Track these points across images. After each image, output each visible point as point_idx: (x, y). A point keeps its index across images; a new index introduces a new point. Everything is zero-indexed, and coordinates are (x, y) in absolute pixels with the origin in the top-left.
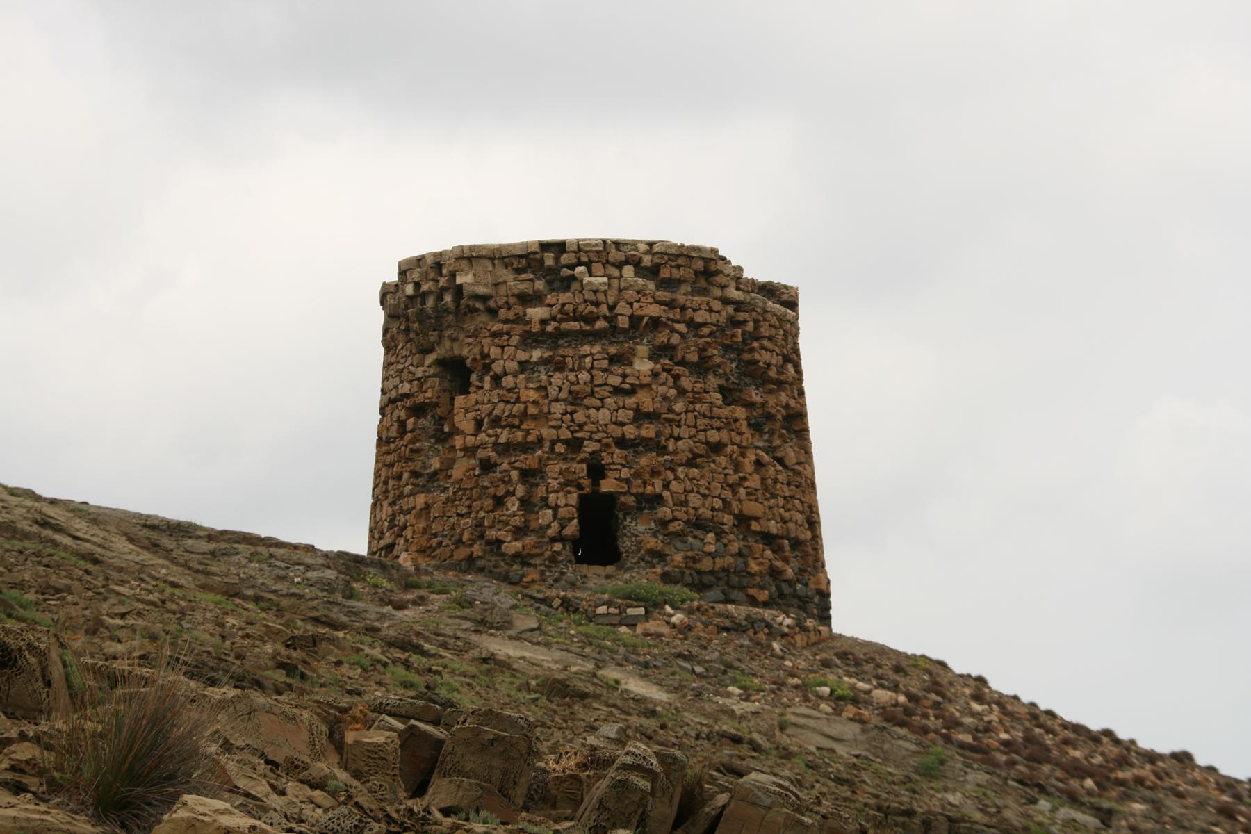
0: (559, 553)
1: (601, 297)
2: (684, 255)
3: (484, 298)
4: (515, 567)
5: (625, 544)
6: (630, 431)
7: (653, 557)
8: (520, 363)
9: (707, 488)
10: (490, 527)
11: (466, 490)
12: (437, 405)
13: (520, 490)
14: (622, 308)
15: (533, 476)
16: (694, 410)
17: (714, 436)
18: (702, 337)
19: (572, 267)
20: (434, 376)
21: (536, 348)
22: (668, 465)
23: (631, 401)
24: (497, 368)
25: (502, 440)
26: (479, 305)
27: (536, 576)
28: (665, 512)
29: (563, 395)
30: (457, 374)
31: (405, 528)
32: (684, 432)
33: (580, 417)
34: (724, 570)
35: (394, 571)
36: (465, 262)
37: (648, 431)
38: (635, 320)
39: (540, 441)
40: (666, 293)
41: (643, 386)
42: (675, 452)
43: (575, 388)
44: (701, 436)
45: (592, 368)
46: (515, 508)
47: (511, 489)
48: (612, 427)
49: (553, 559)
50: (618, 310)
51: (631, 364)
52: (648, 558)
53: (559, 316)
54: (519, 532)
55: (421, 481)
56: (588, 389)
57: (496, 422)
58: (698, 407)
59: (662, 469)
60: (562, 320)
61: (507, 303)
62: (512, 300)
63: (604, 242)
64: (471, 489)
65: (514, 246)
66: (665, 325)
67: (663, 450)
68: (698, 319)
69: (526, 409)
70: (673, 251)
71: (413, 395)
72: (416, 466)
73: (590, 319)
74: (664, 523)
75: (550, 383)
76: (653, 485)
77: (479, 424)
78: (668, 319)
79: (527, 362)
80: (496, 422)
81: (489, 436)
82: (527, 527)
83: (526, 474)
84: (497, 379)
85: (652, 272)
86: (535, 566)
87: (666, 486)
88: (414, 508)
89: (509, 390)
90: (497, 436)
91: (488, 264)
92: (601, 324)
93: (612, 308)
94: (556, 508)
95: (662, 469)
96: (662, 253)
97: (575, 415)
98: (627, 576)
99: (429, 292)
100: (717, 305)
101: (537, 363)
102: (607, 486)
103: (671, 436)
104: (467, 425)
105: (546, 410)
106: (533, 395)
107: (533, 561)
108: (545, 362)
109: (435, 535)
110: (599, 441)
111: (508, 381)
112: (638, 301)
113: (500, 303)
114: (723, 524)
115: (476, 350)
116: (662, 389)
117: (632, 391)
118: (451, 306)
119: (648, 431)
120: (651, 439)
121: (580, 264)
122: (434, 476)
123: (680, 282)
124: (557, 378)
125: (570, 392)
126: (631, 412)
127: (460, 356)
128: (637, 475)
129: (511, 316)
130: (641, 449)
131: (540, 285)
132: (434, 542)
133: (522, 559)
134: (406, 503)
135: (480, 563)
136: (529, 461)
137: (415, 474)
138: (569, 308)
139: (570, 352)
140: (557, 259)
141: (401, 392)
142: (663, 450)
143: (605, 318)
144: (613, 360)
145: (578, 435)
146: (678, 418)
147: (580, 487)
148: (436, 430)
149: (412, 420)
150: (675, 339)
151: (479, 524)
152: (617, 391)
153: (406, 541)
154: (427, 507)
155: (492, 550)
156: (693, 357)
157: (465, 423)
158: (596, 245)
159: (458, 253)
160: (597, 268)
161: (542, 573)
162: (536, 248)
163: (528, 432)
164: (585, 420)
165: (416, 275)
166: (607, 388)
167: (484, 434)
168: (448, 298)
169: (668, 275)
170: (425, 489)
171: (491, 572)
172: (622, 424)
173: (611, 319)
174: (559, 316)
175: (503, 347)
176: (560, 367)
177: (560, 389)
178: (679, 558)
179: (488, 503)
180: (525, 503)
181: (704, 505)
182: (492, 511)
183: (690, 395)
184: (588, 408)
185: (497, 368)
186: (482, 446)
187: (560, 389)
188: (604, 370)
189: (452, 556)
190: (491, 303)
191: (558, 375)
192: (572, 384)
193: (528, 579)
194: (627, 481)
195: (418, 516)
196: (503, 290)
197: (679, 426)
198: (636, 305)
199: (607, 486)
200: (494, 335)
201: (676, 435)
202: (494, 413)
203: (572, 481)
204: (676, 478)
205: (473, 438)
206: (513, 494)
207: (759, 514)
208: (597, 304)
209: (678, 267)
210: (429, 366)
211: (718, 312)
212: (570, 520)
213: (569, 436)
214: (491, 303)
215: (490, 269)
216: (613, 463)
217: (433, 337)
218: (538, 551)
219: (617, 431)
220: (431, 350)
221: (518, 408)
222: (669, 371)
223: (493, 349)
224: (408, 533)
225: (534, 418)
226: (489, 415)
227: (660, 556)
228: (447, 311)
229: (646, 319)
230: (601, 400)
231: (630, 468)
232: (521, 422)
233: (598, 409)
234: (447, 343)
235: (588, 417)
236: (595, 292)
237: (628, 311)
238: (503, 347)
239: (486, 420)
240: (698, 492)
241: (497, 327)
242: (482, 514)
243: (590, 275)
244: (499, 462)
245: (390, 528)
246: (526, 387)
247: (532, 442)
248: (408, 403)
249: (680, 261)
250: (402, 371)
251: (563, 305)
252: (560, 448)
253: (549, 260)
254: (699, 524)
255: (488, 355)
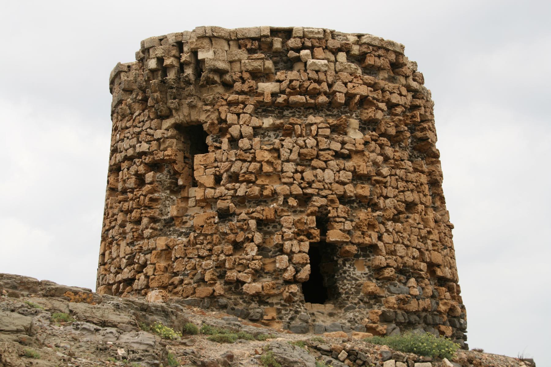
0: (294, 294)
1: (322, 76)
2: (383, 47)
3: (221, 72)
4: (253, 305)
5: (345, 286)
6: (350, 190)
7: (370, 299)
8: (254, 128)
9: (409, 240)
10: (231, 269)
11: (206, 235)
12: (174, 162)
13: (258, 237)
14: (338, 86)
15: (266, 225)
16: (396, 175)
17: (410, 197)
18: (396, 115)
19: (298, 50)
20: (172, 137)
21: (267, 117)
22: (381, 219)
23: (349, 164)
24: (234, 131)
25: (241, 192)
26: (217, 78)
27: (274, 314)
28: (380, 260)
29: (294, 156)
30: (194, 138)
31: (145, 265)
32: (390, 192)
33: (309, 175)
34: (425, 310)
35: (174, 318)
36: (206, 42)
37: (365, 190)
38: (349, 97)
39: (275, 193)
40: (371, 77)
41: (357, 152)
42: (384, 209)
43: (302, 151)
44: (401, 196)
45: (317, 135)
46: (254, 253)
47: (250, 236)
48: (335, 186)
49: (289, 300)
50: (336, 87)
51: (346, 134)
52: (366, 299)
53: (288, 90)
54: (257, 274)
55: (158, 226)
56: (315, 153)
57: (234, 178)
58: (398, 172)
59: (377, 223)
60: (290, 94)
61: (241, 78)
62: (246, 75)
63: (325, 31)
64: (212, 235)
65: (249, 30)
66: (374, 104)
67: (375, 207)
68: (394, 101)
69: (262, 166)
70: (376, 43)
71: (151, 153)
72: (155, 213)
73: (315, 94)
74: (379, 270)
75: (282, 146)
76: (370, 236)
77: (218, 179)
78: (374, 98)
79: (260, 127)
80: (234, 178)
81: (228, 189)
82: (263, 269)
83: (260, 223)
84: (234, 142)
85: (360, 59)
86: (272, 305)
87: (380, 238)
88: (155, 249)
89: (246, 151)
90: (236, 191)
91: (225, 44)
92: (322, 99)
93: (330, 86)
94: (291, 254)
95: (377, 223)
96: (369, 44)
97: (304, 174)
98: (350, 315)
99: (172, 66)
100: (404, 91)
101: (267, 130)
102: (334, 235)
103: (381, 195)
104: (207, 179)
105: (279, 169)
106: (267, 156)
107: (270, 301)
108: (275, 128)
109: (176, 274)
110: (325, 197)
111: (244, 143)
112: (351, 82)
113: (235, 77)
114: (421, 270)
115: (214, 116)
116: (373, 156)
117: (347, 157)
118: (192, 78)
119: (365, 190)
120: (366, 197)
121: (304, 47)
122: (170, 222)
123: (380, 69)
124: (288, 142)
125: (299, 154)
126: (350, 174)
127: (198, 121)
128: (357, 227)
129: (245, 88)
130: (355, 205)
131: (269, 64)
132: (177, 279)
133: (260, 298)
134: (144, 244)
135: (223, 301)
136: (267, 211)
137: (154, 220)
138: (296, 84)
139: (299, 121)
140: (283, 43)
141: (138, 150)
142: (375, 207)
143: (325, 93)
144: (334, 129)
145: (309, 191)
146: (385, 180)
147: (309, 236)
148: (171, 183)
149: (151, 173)
150: (379, 115)
151: (220, 265)
152: (338, 155)
153: (147, 277)
154: (168, 249)
155: (230, 289)
156: (392, 131)
157: (205, 177)
158: (319, 33)
159: (201, 32)
160: (319, 52)
161: (279, 311)
162: (267, 32)
163: (263, 187)
164: (313, 178)
165: (159, 52)
166: (331, 153)
167: (223, 188)
168: (189, 71)
169: (372, 62)
170: (161, 233)
171: (233, 309)
172: (343, 184)
173: (331, 95)
174: (288, 90)
175: (238, 115)
176: (289, 132)
177: (291, 151)
178: (392, 299)
179: (229, 248)
180: (261, 249)
181: (407, 255)
182: (231, 255)
183: (392, 161)
184: (314, 168)
185: (234, 131)
186: (221, 197)
187: (291, 151)
188: (327, 137)
189: (194, 293)
190: (227, 77)
191: (288, 139)
192: (301, 147)
193: (269, 317)
194: (349, 232)
195: (159, 256)
196: (237, 67)
197: (386, 187)
198: (350, 85)
199: (334, 235)
200: (230, 104)
201: (385, 194)
202: (232, 170)
203: (303, 231)
204: (387, 231)
205: (213, 190)
206: (252, 240)
207: (440, 262)
208: (319, 82)
209: (379, 56)
210: (167, 130)
211: (405, 96)
212: (304, 265)
213: (300, 191)
214: (227, 77)
215: (226, 48)
216: (338, 217)
217: (172, 103)
218: (276, 291)
219: (340, 189)
220: (167, 117)
221: (254, 166)
222: (375, 141)
223: (229, 115)
224: (149, 270)
225: (268, 175)
226: (227, 171)
227: (375, 297)
228: (188, 83)
229: (358, 97)
230: (326, 162)
231: (352, 221)
232: (256, 179)
233: (323, 170)
234: (185, 110)
235: (316, 176)
236: (317, 72)
237: (344, 90)
238: (238, 115)
239: (225, 175)
240: (403, 243)
241: (232, 97)
242: (222, 257)
243: (313, 58)
244: (238, 211)
245: (128, 265)
246: (261, 149)
247: (267, 196)
248: (148, 159)
249: (380, 52)
250: (139, 133)
251: (291, 81)
252: (292, 202)
253: (277, 44)
254: (405, 272)
255: (225, 121)
